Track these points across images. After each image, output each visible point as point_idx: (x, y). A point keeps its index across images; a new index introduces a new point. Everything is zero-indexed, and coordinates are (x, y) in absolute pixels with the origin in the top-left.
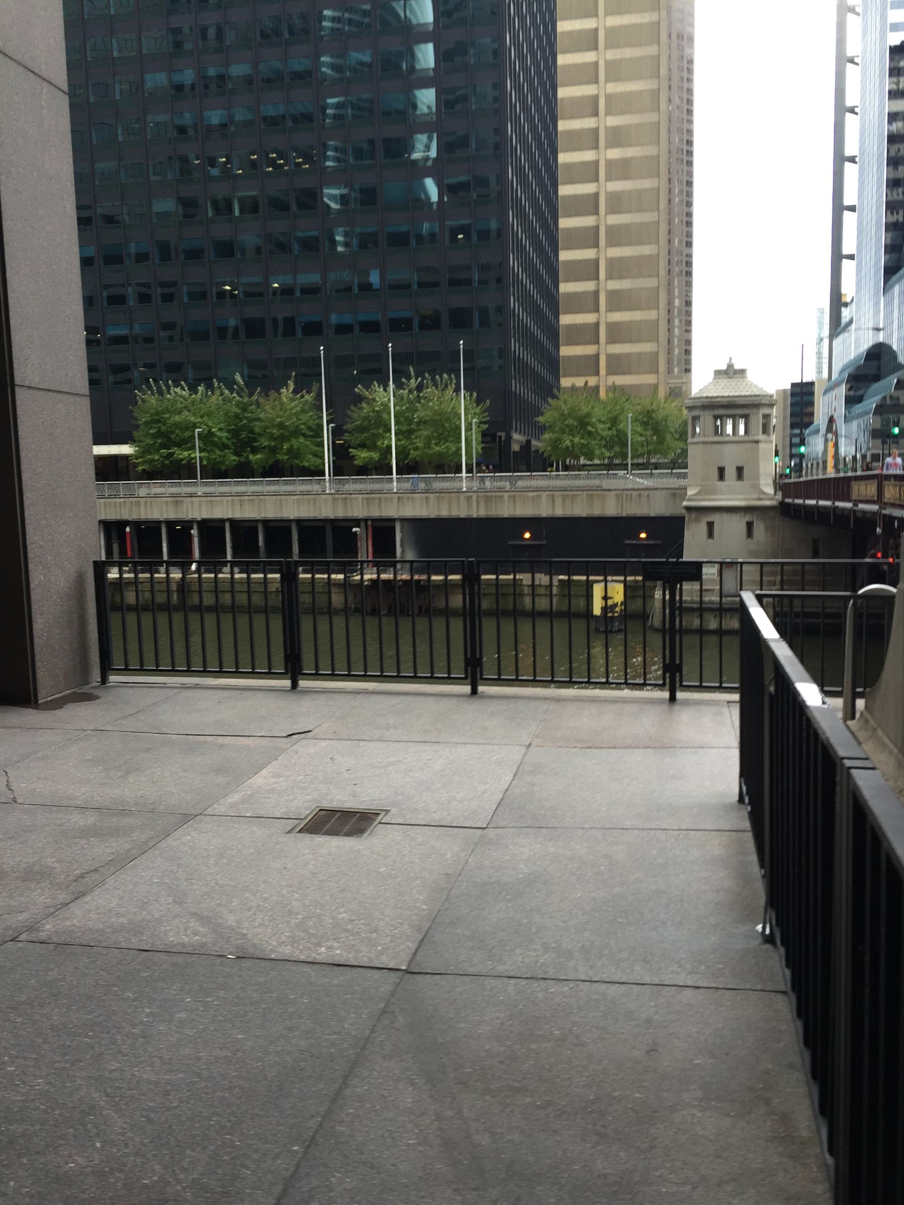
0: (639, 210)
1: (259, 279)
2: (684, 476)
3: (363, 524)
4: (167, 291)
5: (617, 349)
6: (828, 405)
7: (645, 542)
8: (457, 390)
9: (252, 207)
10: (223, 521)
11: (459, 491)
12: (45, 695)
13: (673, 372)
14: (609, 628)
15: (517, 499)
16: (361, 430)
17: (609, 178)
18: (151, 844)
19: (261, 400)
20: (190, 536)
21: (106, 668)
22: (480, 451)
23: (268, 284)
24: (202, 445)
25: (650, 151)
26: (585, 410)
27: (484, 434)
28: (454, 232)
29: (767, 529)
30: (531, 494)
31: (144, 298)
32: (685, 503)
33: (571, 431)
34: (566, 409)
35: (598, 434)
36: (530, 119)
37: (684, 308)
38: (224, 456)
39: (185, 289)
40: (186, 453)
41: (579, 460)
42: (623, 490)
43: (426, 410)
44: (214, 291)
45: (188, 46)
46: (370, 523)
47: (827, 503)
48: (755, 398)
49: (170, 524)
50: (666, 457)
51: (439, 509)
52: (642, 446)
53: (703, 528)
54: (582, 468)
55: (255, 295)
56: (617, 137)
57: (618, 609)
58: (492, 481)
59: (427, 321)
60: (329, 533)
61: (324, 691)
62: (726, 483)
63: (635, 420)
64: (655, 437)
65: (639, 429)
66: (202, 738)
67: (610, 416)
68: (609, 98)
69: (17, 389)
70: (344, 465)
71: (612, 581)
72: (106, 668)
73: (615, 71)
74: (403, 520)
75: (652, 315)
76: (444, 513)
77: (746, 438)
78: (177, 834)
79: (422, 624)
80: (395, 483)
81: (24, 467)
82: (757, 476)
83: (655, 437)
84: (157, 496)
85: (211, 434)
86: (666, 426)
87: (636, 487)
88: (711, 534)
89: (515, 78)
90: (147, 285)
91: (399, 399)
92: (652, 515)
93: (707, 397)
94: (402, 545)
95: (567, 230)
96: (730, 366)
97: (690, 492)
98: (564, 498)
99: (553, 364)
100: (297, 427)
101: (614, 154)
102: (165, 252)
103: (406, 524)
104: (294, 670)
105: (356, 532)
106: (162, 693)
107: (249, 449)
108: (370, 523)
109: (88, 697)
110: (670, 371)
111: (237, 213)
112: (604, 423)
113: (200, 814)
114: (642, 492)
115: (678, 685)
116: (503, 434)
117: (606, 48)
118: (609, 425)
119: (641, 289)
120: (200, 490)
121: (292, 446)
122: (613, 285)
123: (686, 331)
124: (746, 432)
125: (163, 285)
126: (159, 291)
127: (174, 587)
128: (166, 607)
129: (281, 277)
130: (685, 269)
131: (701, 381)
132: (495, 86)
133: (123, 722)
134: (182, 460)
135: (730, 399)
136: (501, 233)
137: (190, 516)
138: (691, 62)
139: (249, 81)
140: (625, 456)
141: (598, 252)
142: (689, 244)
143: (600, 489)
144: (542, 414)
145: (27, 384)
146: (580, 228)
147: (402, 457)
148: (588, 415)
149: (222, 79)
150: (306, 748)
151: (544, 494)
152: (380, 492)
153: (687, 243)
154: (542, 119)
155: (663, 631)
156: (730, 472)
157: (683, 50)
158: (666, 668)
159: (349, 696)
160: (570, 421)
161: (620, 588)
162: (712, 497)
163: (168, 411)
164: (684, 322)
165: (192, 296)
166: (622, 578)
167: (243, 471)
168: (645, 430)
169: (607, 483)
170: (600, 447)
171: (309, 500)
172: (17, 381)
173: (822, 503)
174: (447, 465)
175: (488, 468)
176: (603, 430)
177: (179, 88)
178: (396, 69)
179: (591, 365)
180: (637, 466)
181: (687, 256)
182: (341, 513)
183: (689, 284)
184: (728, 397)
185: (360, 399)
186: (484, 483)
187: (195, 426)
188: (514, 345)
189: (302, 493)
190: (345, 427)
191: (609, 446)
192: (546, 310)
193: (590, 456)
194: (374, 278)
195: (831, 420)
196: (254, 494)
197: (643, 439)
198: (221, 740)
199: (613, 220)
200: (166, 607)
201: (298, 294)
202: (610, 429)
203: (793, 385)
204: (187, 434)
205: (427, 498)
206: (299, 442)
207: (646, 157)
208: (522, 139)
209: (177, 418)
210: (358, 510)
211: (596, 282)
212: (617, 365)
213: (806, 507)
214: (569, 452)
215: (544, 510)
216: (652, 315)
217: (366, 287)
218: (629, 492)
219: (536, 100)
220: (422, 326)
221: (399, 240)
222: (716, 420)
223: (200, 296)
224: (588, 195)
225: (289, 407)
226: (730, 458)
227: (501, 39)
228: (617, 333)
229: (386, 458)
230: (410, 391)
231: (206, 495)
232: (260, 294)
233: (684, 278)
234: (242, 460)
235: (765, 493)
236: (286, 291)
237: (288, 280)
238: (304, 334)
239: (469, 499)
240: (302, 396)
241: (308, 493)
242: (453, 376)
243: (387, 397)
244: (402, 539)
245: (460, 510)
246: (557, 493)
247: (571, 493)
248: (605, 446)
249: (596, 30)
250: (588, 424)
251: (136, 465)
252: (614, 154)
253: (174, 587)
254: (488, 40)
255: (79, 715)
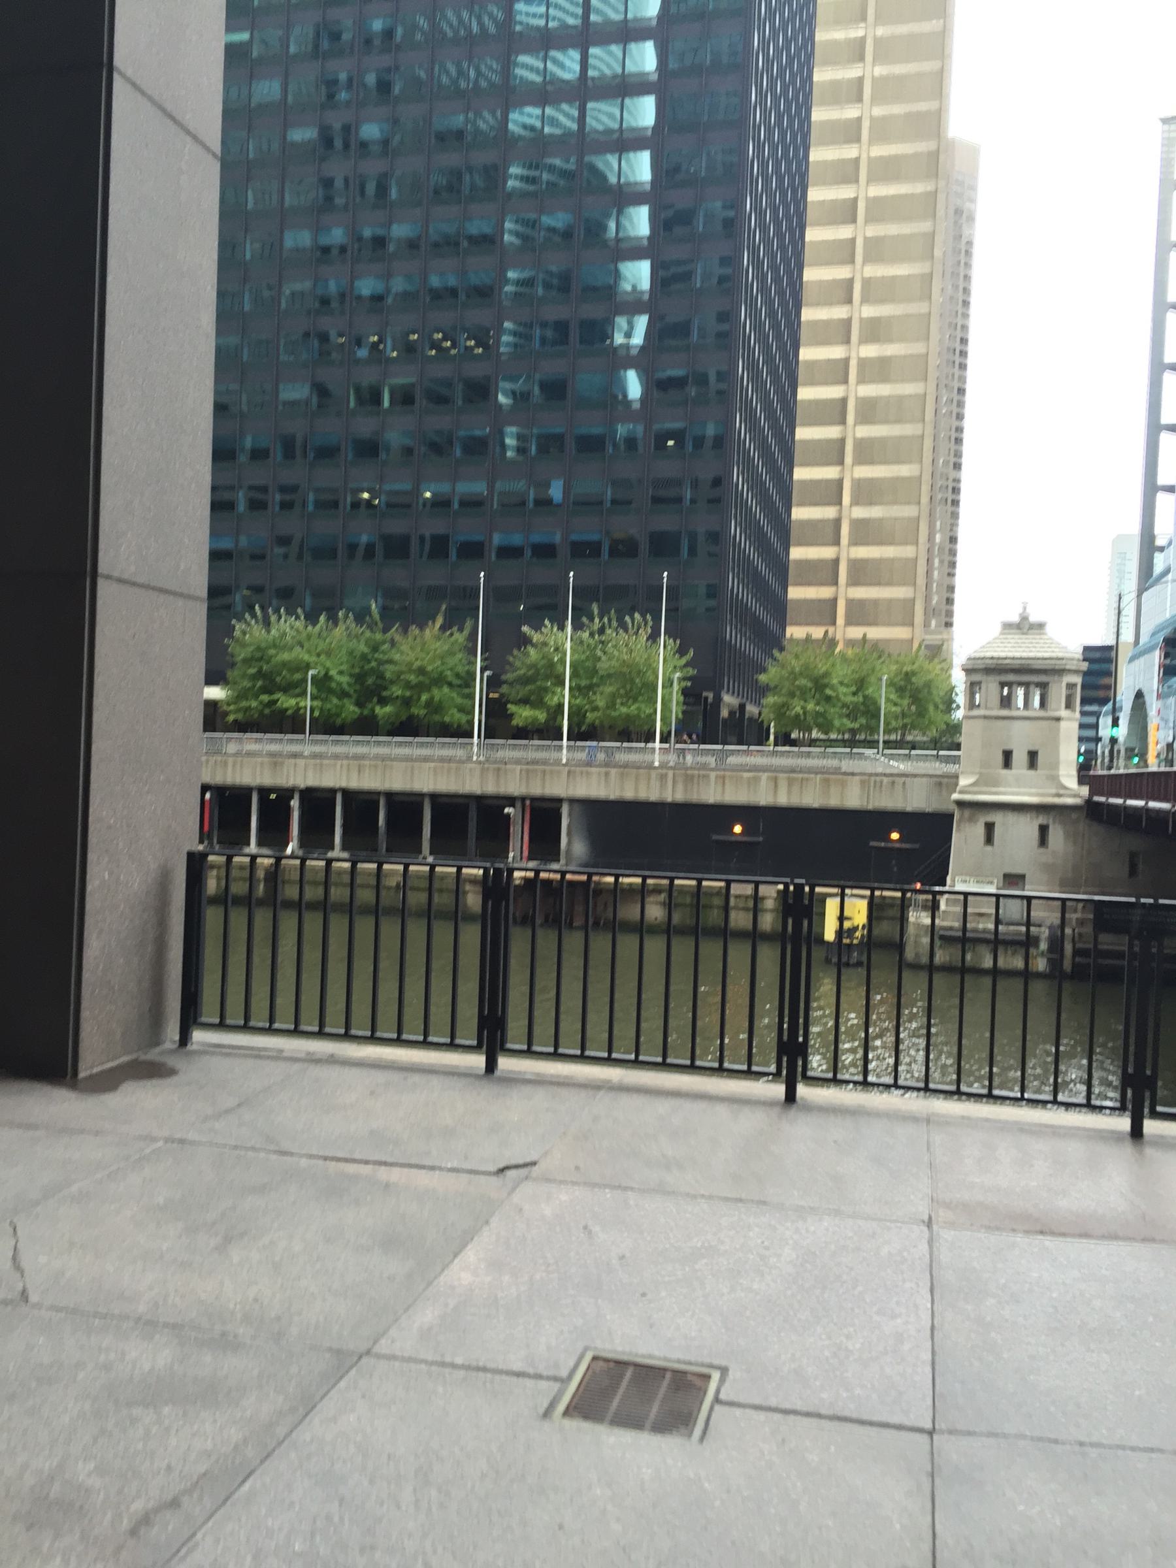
0: (898, 421)
1: (407, 486)
2: (956, 760)
3: (519, 804)
4: (288, 497)
5: (860, 593)
6: (1137, 675)
7: (897, 845)
8: (654, 637)
9: (405, 398)
10: (333, 791)
11: (650, 766)
12: (90, 1063)
13: (929, 626)
14: (844, 959)
15: (727, 781)
16: (525, 681)
17: (861, 380)
18: (281, 1431)
19: (397, 638)
20: (288, 810)
21: (190, 1019)
22: (680, 716)
23: (417, 492)
24: (315, 691)
25: (918, 348)
26: (822, 668)
27: (685, 692)
28: (661, 438)
29: (1067, 835)
30: (746, 775)
31: (257, 505)
32: (955, 796)
33: (803, 694)
34: (797, 665)
35: (839, 700)
36: (769, 302)
37: (948, 546)
38: (343, 706)
39: (311, 497)
40: (292, 702)
41: (810, 733)
42: (871, 775)
43: (609, 659)
44: (349, 500)
45: (339, 201)
46: (528, 802)
47: (1140, 803)
48: (1058, 662)
49: (264, 792)
50: (924, 734)
51: (622, 789)
52: (896, 718)
53: (979, 830)
54: (813, 743)
55: (401, 505)
56: (875, 331)
57: (858, 934)
58: (697, 755)
59: (620, 547)
60: (473, 814)
61: (539, 1081)
62: (1014, 771)
63: (891, 684)
64: (913, 708)
65: (893, 696)
66: (351, 1168)
67: (856, 676)
68: (867, 282)
69: (101, 583)
70: (499, 725)
71: (853, 895)
72: (190, 1019)
73: (877, 251)
74: (573, 801)
75: (908, 551)
76: (629, 794)
77: (1042, 714)
78: (328, 1407)
79: (601, 943)
80: (565, 751)
81: (97, 701)
82: (1055, 765)
83: (913, 708)
84: (250, 754)
85: (327, 677)
86: (930, 693)
87: (888, 771)
88: (989, 840)
89: (754, 252)
90: (264, 489)
91: (577, 643)
92: (909, 809)
93: (992, 658)
94: (569, 834)
95: (804, 442)
96: (1024, 618)
97: (964, 782)
98: (791, 782)
99: (780, 609)
100: (441, 673)
101: (870, 351)
102: (289, 448)
103: (576, 807)
104: (492, 1039)
105: (508, 815)
106: (277, 1070)
107: (375, 700)
108: (528, 802)
109: (154, 1071)
110: (926, 625)
111: (386, 404)
112: (847, 686)
113: (368, 1352)
114: (897, 779)
115: (1146, 1111)
116: (710, 695)
117: (866, 222)
118: (854, 689)
119: (896, 519)
120: (308, 750)
121: (432, 698)
122: (859, 512)
123: (949, 574)
124: (1043, 704)
125: (283, 489)
126: (278, 497)
127: (261, 874)
128: (247, 902)
129: (433, 486)
130: (950, 497)
131: (974, 635)
132: (724, 261)
133: (217, 1125)
134: (286, 710)
135: (1023, 662)
136: (720, 442)
137: (291, 783)
138: (970, 243)
139: (412, 245)
140: (874, 730)
141: (842, 471)
142: (957, 466)
143: (837, 771)
144: (764, 670)
145: (116, 574)
146: (819, 441)
147: (575, 719)
148: (826, 674)
149: (380, 242)
150: (543, 1204)
151: (764, 776)
152: (545, 762)
153: (955, 464)
154: (783, 303)
155: (777, 937)
156: (1020, 758)
157: (961, 227)
158: (1127, 1081)
159: (583, 1093)
160: (803, 682)
161: (863, 905)
162: (994, 789)
163: (275, 646)
164: (946, 564)
165: (319, 504)
166: (868, 893)
167: (366, 727)
168: (901, 697)
169: (846, 765)
170: (841, 716)
171: (449, 770)
172: (103, 568)
173: (1153, 804)
174: (635, 732)
175: (690, 737)
176: (845, 694)
177: (326, 250)
178: (593, 241)
179: (825, 612)
180: (888, 744)
181: (954, 480)
182: (490, 788)
183: (955, 516)
184: (1021, 658)
185: (526, 641)
186: (684, 758)
187: (308, 667)
188: (732, 582)
189: (442, 760)
190: (504, 677)
191: (852, 714)
192: (774, 539)
193: (826, 728)
194: (556, 492)
195: (1139, 695)
196: (377, 757)
197: (898, 709)
198: (383, 1173)
199: (863, 431)
200: (247, 902)
201: (456, 506)
202: (854, 694)
203: (1087, 649)
204: (297, 676)
205: (607, 774)
206: (441, 693)
207: (911, 356)
208: (758, 326)
209: (286, 656)
210: (513, 786)
211: (838, 508)
212: (860, 613)
213: (1126, 808)
214: (800, 722)
215: (763, 796)
216: (908, 551)
217: (544, 503)
218: (878, 779)
219: (777, 280)
220: (613, 552)
221: (591, 445)
222: (1002, 688)
223: (329, 505)
224: (832, 401)
225: (433, 647)
226: (1020, 737)
227: (737, 205)
228: (861, 573)
229: (555, 719)
230: (592, 635)
231: (314, 756)
232: (409, 506)
233: (949, 508)
234: (366, 712)
235: (1065, 788)
236: (441, 504)
237: (445, 488)
238: (459, 556)
239: (663, 778)
240: (452, 635)
241: (450, 760)
242: (649, 617)
243: (563, 642)
244: (569, 826)
245: (650, 791)
246: (781, 775)
247: (800, 776)
248: (848, 716)
249: (855, 200)
250: (826, 686)
251: (226, 714)
252: (870, 351)
253: (261, 874)
254: (719, 204)
255: (139, 1100)
